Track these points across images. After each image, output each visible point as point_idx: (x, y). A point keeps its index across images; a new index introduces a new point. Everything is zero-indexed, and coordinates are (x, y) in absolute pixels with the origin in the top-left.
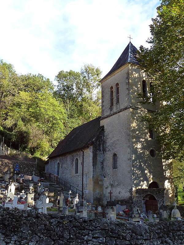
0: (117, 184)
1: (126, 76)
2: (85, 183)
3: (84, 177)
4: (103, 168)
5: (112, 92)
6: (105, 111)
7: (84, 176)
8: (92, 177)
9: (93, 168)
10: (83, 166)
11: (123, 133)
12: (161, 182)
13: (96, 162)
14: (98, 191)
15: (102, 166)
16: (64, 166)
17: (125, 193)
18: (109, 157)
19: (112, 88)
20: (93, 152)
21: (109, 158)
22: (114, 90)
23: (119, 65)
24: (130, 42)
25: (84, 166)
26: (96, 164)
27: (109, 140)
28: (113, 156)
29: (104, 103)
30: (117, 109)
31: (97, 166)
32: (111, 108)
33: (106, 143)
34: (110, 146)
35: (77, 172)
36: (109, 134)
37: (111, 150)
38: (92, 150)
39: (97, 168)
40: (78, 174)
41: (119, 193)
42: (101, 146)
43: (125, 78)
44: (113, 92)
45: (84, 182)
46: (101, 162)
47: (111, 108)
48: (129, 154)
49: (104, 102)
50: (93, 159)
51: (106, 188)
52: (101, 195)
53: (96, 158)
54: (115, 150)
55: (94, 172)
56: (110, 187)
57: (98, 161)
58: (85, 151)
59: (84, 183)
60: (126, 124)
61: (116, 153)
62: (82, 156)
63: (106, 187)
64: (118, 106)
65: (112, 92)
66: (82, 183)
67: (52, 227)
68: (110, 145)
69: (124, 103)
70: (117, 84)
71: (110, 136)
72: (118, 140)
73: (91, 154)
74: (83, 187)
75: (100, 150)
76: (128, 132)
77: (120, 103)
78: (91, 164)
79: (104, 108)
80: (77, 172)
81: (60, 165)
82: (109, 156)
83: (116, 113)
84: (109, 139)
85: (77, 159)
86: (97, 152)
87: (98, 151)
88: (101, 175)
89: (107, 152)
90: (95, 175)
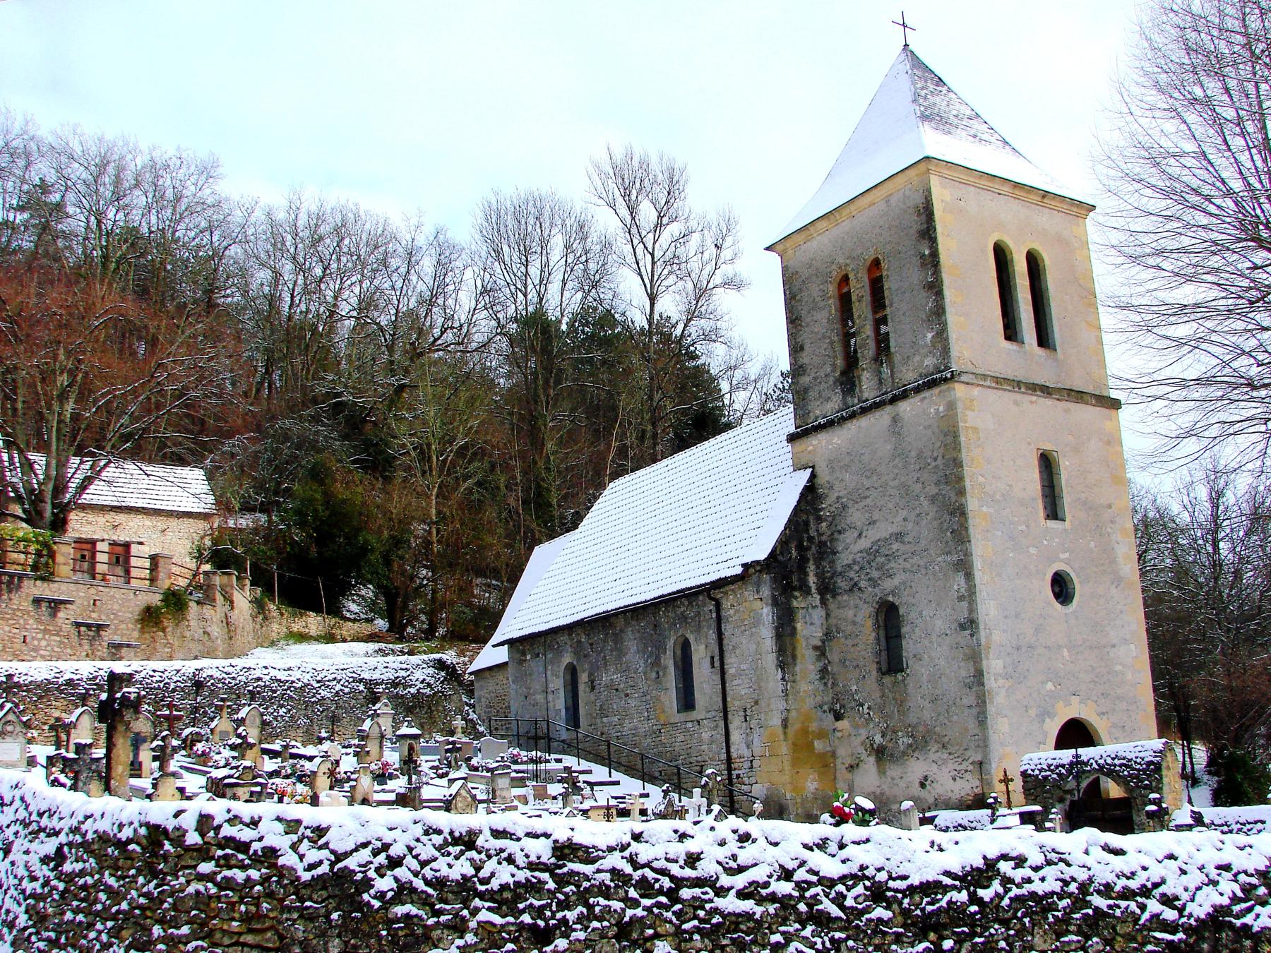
1: (916, 224)
3: (731, 727)
5: (845, 301)
6: (812, 394)
7: (736, 722)
8: (776, 721)
9: (783, 679)
10: (723, 673)
11: (925, 503)
12: (1105, 717)
13: (794, 649)
15: (820, 665)
17: (954, 779)
18: (858, 619)
19: (845, 280)
20: (775, 603)
21: (854, 623)
22: (860, 289)
24: (906, 45)
25: (731, 671)
26: (794, 657)
27: (849, 536)
28: (877, 613)
29: (804, 354)
30: (881, 383)
31: (798, 669)
32: (848, 380)
34: (856, 568)
35: (687, 701)
36: (844, 507)
37: (862, 584)
38: (766, 591)
39: (798, 678)
40: (694, 715)
42: (811, 568)
43: (913, 231)
44: (854, 298)
46: (816, 648)
47: (848, 380)
48: (961, 598)
49: (802, 348)
54: (888, 584)
56: (872, 759)
59: (734, 755)
60: (935, 459)
61: (890, 599)
62: (713, 624)
63: (849, 761)
64: (885, 369)
65: (845, 301)
66: (724, 756)
67: (185, 930)
68: (854, 562)
69: (917, 358)
70: (876, 263)
71: (856, 516)
72: (899, 536)
73: (767, 614)
74: (730, 775)
75: (806, 591)
76: (953, 495)
77: (897, 358)
78: (770, 660)
79: (805, 380)
80: (687, 701)
81: (583, 677)
82: (857, 615)
83: (877, 406)
84: (847, 534)
87: (797, 594)
88: (821, 707)
89: (839, 598)
90: (793, 714)
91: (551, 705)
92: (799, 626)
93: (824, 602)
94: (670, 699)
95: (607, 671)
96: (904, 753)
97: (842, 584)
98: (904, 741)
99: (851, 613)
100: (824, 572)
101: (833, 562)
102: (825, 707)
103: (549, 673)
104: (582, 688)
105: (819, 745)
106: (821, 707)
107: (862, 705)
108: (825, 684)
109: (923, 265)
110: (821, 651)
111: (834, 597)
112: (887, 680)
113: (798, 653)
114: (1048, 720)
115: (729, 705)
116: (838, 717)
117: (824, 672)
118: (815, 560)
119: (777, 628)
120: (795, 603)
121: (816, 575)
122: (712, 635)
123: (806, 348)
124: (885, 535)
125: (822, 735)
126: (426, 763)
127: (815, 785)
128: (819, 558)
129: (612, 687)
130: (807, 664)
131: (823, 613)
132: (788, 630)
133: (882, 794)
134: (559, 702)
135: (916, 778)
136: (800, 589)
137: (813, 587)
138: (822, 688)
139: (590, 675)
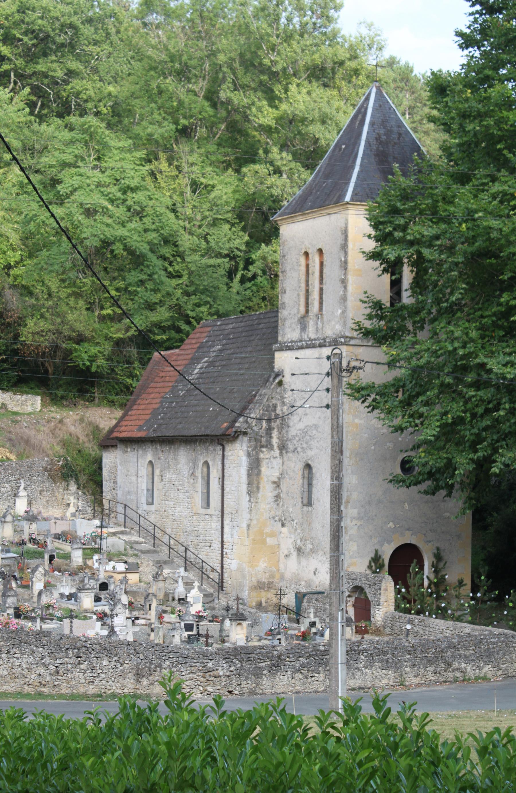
0: (311, 550)
1: (340, 241)
2: (230, 540)
4: (280, 498)
8: (244, 525)
9: (250, 501)
13: (258, 483)
14: (262, 565)
15: (276, 493)
16: (169, 475)
20: (249, 455)
21: (294, 471)
23: (360, 117)
26: (258, 488)
31: (260, 495)
33: (289, 427)
34: (297, 439)
38: (245, 447)
39: (260, 500)
40: (209, 511)
41: (315, 573)
42: (275, 434)
45: (225, 536)
46: (274, 482)
49: (285, 292)
50: (249, 475)
51: (286, 556)
52: (272, 576)
53: (259, 473)
54: (310, 453)
55: (253, 512)
57: (265, 479)
58: (229, 448)
63: (286, 552)
73: (244, 461)
77: (325, 318)
78: (244, 488)
81: (157, 472)
85: (206, 463)
86: (263, 452)
87: (264, 449)
90: (254, 522)
91: (139, 485)
92: (263, 469)
93: (281, 454)
94: (198, 499)
95: (169, 472)
96: (308, 554)
97: (291, 447)
98: (309, 546)
99: (293, 465)
100: (283, 437)
101: (287, 432)
102: (277, 518)
103: (139, 464)
104: (156, 479)
105: (270, 541)
106: (273, 518)
107: (293, 520)
108: (278, 504)
109: (341, 266)
110: (277, 484)
111: (287, 452)
112: (305, 508)
113: (261, 486)
114: (386, 544)
115: (225, 509)
116: (283, 525)
117: (277, 497)
118: (278, 429)
119: (248, 471)
120: (262, 456)
121: (278, 438)
122: (220, 463)
123: (287, 292)
124: (310, 424)
125: (272, 535)
126: (131, 79)
127: (265, 564)
128: (280, 429)
129: (171, 482)
130: (267, 491)
131: (281, 461)
132: (256, 472)
133: (298, 574)
134: (143, 485)
135: (312, 569)
136: (266, 446)
137: (275, 447)
138: (275, 506)
139: (161, 471)
